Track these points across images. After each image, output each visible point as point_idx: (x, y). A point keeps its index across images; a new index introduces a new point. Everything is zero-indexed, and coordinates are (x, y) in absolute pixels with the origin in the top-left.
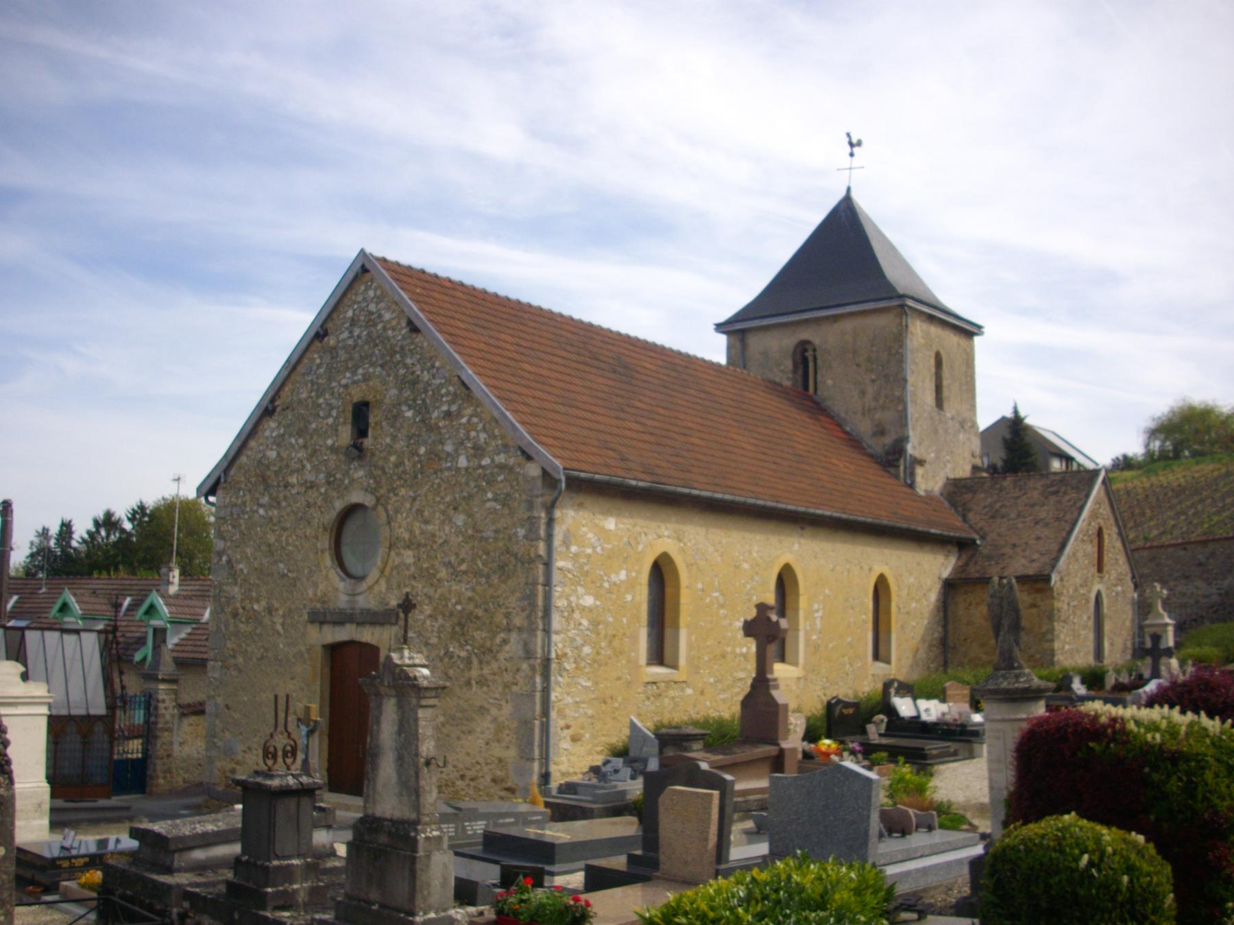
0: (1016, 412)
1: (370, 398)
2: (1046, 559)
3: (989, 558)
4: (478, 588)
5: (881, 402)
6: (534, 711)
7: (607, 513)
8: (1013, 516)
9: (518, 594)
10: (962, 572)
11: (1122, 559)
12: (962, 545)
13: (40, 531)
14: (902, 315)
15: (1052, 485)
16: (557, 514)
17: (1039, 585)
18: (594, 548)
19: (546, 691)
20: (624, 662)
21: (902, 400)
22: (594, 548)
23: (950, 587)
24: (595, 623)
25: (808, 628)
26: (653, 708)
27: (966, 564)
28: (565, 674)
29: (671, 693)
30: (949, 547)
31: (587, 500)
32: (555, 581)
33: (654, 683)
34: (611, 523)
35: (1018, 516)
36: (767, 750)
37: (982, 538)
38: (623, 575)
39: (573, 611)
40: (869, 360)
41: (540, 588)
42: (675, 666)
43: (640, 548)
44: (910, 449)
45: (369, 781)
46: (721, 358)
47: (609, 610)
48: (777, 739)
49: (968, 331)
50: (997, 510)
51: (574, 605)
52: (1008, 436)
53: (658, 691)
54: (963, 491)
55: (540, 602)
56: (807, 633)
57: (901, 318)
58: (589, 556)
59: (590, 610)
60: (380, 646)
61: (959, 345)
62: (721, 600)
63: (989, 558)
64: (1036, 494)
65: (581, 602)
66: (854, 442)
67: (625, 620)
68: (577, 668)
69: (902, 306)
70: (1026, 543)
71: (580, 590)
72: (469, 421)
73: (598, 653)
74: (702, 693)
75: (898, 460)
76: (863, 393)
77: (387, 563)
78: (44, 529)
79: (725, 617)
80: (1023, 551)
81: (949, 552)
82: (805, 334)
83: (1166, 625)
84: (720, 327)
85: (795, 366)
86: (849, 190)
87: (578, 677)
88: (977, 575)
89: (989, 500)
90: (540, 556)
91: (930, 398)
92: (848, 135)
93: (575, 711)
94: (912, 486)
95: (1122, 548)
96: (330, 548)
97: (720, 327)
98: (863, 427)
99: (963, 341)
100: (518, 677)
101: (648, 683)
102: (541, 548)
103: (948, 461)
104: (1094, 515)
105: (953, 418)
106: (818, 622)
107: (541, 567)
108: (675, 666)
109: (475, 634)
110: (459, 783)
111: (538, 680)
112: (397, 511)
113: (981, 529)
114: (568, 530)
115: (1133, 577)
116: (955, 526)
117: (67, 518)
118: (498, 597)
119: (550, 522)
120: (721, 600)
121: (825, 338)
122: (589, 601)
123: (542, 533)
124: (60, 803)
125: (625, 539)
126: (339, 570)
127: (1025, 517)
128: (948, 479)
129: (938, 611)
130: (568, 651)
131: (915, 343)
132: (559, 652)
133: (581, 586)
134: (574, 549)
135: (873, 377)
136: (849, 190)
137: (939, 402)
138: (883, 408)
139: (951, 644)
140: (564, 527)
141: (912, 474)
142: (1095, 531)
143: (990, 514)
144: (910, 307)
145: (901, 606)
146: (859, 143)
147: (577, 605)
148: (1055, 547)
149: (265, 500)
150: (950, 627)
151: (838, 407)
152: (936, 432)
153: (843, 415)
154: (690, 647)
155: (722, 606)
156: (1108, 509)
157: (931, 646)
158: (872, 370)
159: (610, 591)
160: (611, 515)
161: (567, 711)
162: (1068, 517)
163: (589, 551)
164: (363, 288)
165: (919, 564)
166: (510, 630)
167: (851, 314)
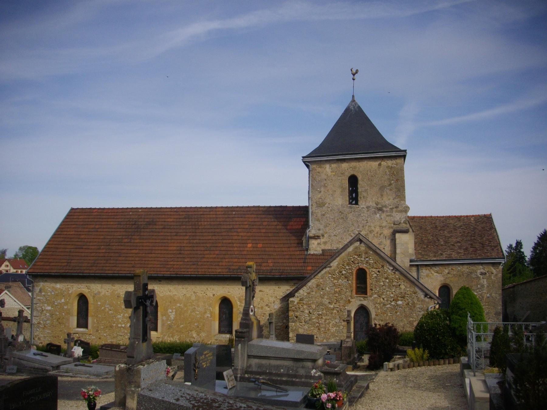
7: (56, 283)
13: (509, 246)
20: (63, 326)
24: (52, 315)
38: (63, 300)
43: (70, 292)
45: (97, 364)
65: (46, 308)
67: (64, 314)
71: (46, 305)
78: (510, 245)
86: (353, 96)
117: (519, 239)
122: (49, 308)
124: (350, 404)
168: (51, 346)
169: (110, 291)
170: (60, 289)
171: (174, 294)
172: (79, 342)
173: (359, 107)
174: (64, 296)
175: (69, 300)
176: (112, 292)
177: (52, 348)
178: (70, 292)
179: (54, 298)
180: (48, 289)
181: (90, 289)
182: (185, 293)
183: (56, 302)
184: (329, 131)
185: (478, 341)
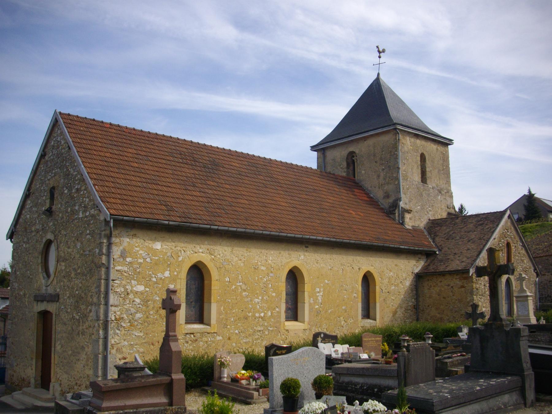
0: (530, 192)
1: (55, 185)
2: (469, 261)
3: (441, 261)
4: (83, 282)
5: (387, 180)
6: (99, 349)
7: (155, 240)
8: (458, 238)
9: (95, 285)
10: (426, 269)
11: (526, 260)
12: (429, 255)
14: (396, 134)
15: (481, 220)
16: (114, 240)
17: (465, 276)
18: (145, 259)
19: (106, 338)
21: (397, 179)
22: (145, 259)
23: (419, 277)
25: (312, 302)
26: (191, 347)
27: (429, 265)
28: (122, 329)
29: (205, 339)
30: (420, 256)
31: (140, 233)
32: (112, 277)
33: (193, 334)
34: (158, 246)
35: (460, 238)
36: (164, 379)
37: (440, 250)
38: (167, 274)
39: (128, 294)
40: (381, 159)
41: (103, 281)
42: (209, 325)
43: (180, 259)
44: (402, 204)
46: (314, 166)
47: (156, 293)
48: (171, 373)
49: (445, 143)
50: (451, 235)
51: (129, 291)
52: (526, 204)
53: (195, 338)
54: (436, 226)
55: (103, 289)
56: (310, 304)
57: (396, 136)
58: (141, 263)
59: (142, 293)
60: (53, 313)
61: (437, 149)
62: (244, 287)
63: (441, 261)
64: (471, 226)
65: (135, 289)
66: (373, 202)
68: (131, 325)
69: (396, 129)
70: (461, 252)
72: (83, 193)
73: (147, 317)
74: (229, 339)
75: (394, 210)
76: (379, 176)
77: (56, 269)
79: (247, 297)
80: (459, 257)
81: (420, 258)
82: (351, 149)
83: (527, 296)
84: (313, 148)
85: (348, 165)
86: (378, 74)
87: (132, 330)
88: (433, 271)
89: (448, 230)
90: (103, 264)
91: (417, 177)
92: (377, 47)
93: (130, 350)
94: (402, 224)
95: (526, 254)
96: (41, 263)
97: (313, 148)
98: (379, 194)
99: (441, 148)
100: (94, 330)
101: (187, 334)
102: (104, 259)
103: (430, 211)
104: (503, 235)
105: (433, 188)
106: (320, 298)
107: (103, 270)
108: (209, 325)
109: (82, 307)
110: (75, 387)
111: (101, 332)
112: (61, 243)
113: (441, 246)
114: (124, 249)
115: (535, 269)
116: (429, 243)
118: (89, 286)
119: (110, 245)
120: (244, 287)
121: (360, 149)
122: (141, 288)
123: (104, 251)
125: (169, 254)
126: (44, 274)
127: (463, 238)
128: (429, 220)
129: (412, 291)
130: (125, 316)
131: (406, 149)
132: (117, 317)
133: (135, 280)
134: (128, 260)
135: (383, 168)
136: (378, 74)
137: (424, 179)
138: (388, 183)
139: (422, 309)
140: (121, 248)
141: (403, 218)
142: (505, 245)
143: (447, 237)
144: (399, 129)
145: (384, 289)
146: (384, 51)
147: (131, 291)
148: (476, 254)
149: (25, 240)
150: (421, 299)
151: (367, 185)
152: (421, 195)
153: (370, 189)
154: (219, 313)
155: (245, 291)
156: (514, 232)
157: (406, 310)
158: (382, 164)
159: (156, 283)
160: (158, 241)
161: (124, 349)
162: (486, 236)
163: (141, 261)
164: (57, 129)
165: (396, 265)
166: (92, 305)
167: (372, 136)
172: (322, 336)
175: (179, 272)
178: (180, 259)
180: (138, 251)
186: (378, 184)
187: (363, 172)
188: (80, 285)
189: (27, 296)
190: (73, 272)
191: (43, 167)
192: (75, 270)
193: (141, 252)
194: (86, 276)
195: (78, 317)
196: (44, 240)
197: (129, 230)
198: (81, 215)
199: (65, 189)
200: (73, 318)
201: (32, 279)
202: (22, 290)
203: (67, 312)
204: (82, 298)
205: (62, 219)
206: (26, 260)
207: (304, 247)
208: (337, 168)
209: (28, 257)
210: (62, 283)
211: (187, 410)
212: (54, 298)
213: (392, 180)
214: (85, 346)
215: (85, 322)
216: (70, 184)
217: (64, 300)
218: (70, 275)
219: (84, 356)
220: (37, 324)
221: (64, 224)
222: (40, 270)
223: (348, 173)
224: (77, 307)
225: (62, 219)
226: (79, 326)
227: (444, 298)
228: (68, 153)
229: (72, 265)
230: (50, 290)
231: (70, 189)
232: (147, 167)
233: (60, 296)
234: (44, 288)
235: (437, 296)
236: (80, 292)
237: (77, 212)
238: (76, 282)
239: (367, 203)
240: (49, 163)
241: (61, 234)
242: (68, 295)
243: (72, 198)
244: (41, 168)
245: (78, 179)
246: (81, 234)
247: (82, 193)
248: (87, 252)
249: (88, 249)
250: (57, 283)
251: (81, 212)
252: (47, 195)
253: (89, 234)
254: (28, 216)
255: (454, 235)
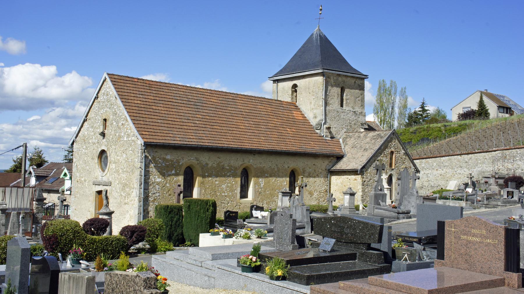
43: (181, 163)
50: (355, 145)
143: (352, 146)
149: (84, 147)
163: (160, 165)
168: (229, 213)
169: (216, 163)
170: (171, 160)
171: (263, 166)
172: (255, 207)
173: (325, 35)
174: (174, 167)
175: (180, 171)
176: (218, 163)
177: (231, 215)
178: (181, 163)
179: (165, 169)
180: (158, 160)
181: (199, 161)
182: (270, 165)
183: (166, 173)
184: (307, 39)
185: (271, 279)
186: (310, 108)
187: (301, 99)
188: (126, 178)
189: (87, 181)
190: (121, 170)
191: (97, 104)
192: (122, 169)
193: (160, 160)
194: (129, 173)
195: (124, 195)
196: (100, 150)
197: (154, 149)
198: (125, 139)
199: (114, 122)
200: (121, 195)
201: (91, 171)
202: (83, 178)
203: (117, 192)
204: (127, 184)
205: (112, 139)
206: (86, 159)
207: (253, 155)
208: (285, 94)
209: (87, 158)
210: (113, 176)
211: (199, 198)
212: (109, 184)
213: (319, 106)
214: (129, 210)
215: (129, 198)
216: (118, 119)
217: (115, 185)
218: (119, 172)
219: (128, 216)
220: (95, 198)
221: (114, 142)
222: (97, 167)
223: (292, 99)
224: (123, 189)
225: (112, 139)
226: (125, 200)
227: (345, 186)
228: (115, 101)
229: (120, 166)
230: (105, 179)
231: (117, 123)
232: (160, 108)
233: (112, 183)
234: (101, 177)
235: (341, 184)
236: (126, 181)
237: (123, 137)
238: (123, 176)
239: (80, 286)
240: (101, 103)
241: (112, 147)
242: (117, 183)
243: (120, 128)
244: (95, 105)
245: (123, 118)
246: (126, 149)
247: (126, 126)
248: (130, 160)
249: (131, 158)
250: (110, 175)
251: (125, 137)
252: (100, 123)
253: (131, 150)
254: (86, 133)
255: (357, 145)
